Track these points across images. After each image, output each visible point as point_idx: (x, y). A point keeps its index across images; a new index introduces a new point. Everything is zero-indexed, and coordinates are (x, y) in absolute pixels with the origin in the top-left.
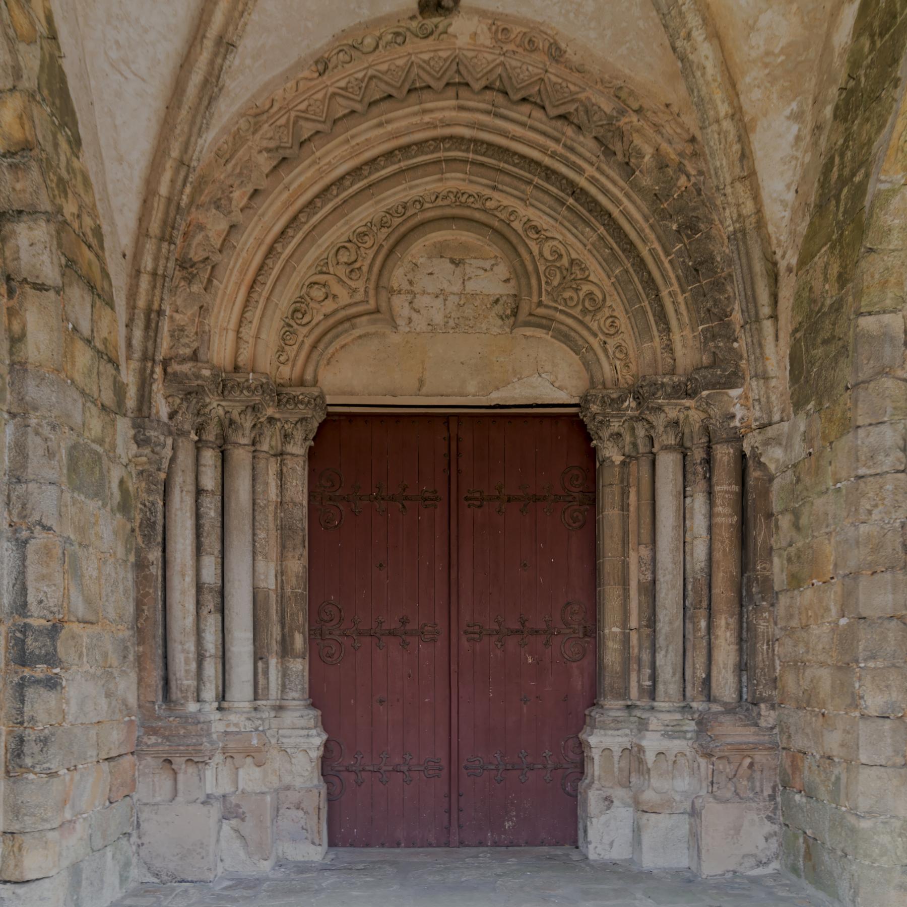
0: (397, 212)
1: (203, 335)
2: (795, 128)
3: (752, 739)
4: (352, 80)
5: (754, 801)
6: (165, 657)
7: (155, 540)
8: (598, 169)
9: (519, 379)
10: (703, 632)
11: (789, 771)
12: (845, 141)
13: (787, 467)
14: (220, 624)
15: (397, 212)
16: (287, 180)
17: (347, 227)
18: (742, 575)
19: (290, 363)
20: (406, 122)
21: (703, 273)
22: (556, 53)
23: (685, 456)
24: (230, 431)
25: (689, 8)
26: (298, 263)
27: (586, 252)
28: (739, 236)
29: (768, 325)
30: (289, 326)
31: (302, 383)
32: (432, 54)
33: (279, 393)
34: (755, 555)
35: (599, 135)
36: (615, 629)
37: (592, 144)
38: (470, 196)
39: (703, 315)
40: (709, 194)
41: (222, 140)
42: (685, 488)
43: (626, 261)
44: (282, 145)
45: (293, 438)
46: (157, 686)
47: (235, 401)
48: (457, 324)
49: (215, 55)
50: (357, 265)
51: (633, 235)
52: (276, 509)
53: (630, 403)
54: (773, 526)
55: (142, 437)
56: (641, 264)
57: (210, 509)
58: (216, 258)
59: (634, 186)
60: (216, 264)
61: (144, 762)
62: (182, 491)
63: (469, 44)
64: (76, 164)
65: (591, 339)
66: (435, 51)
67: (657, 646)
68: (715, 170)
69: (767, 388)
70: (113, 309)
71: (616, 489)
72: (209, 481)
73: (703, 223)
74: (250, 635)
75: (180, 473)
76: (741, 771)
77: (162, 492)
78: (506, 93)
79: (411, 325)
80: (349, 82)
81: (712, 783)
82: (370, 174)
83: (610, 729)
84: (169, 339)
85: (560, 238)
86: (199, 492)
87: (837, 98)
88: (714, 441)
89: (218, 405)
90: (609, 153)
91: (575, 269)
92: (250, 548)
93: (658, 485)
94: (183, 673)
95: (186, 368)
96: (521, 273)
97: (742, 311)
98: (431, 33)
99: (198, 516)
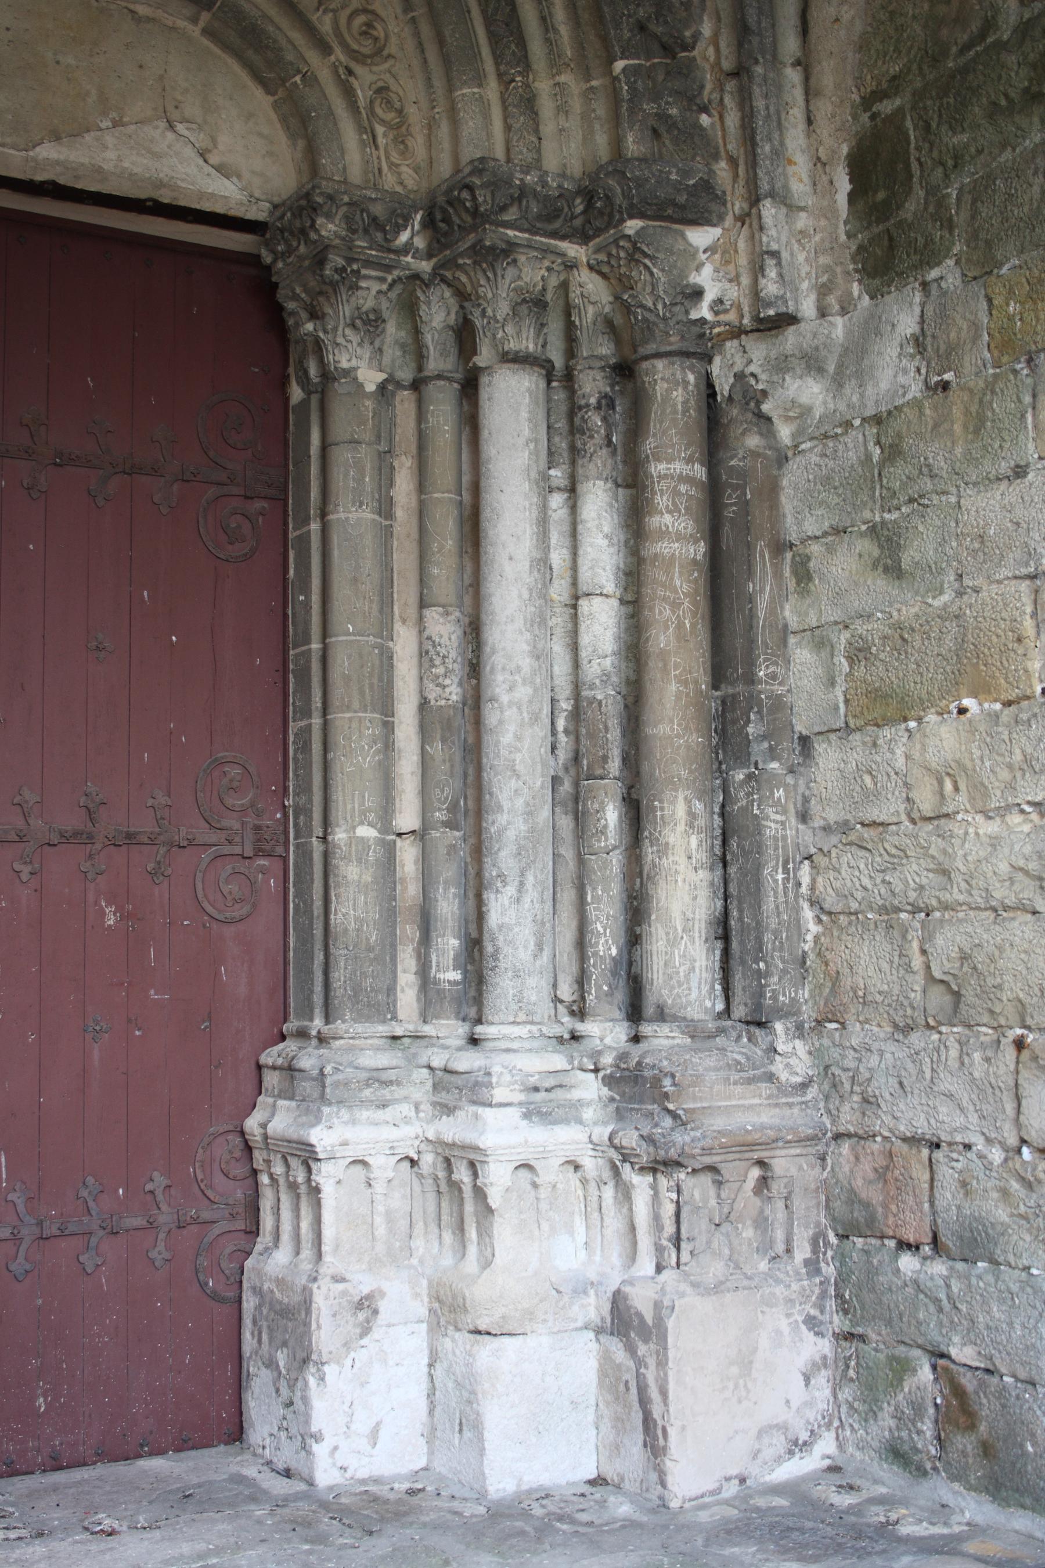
5: (778, 1281)
9: (116, 124)
13: (848, 424)
34: (751, 642)
39: (627, 34)
65: (313, 57)
71: (366, 454)
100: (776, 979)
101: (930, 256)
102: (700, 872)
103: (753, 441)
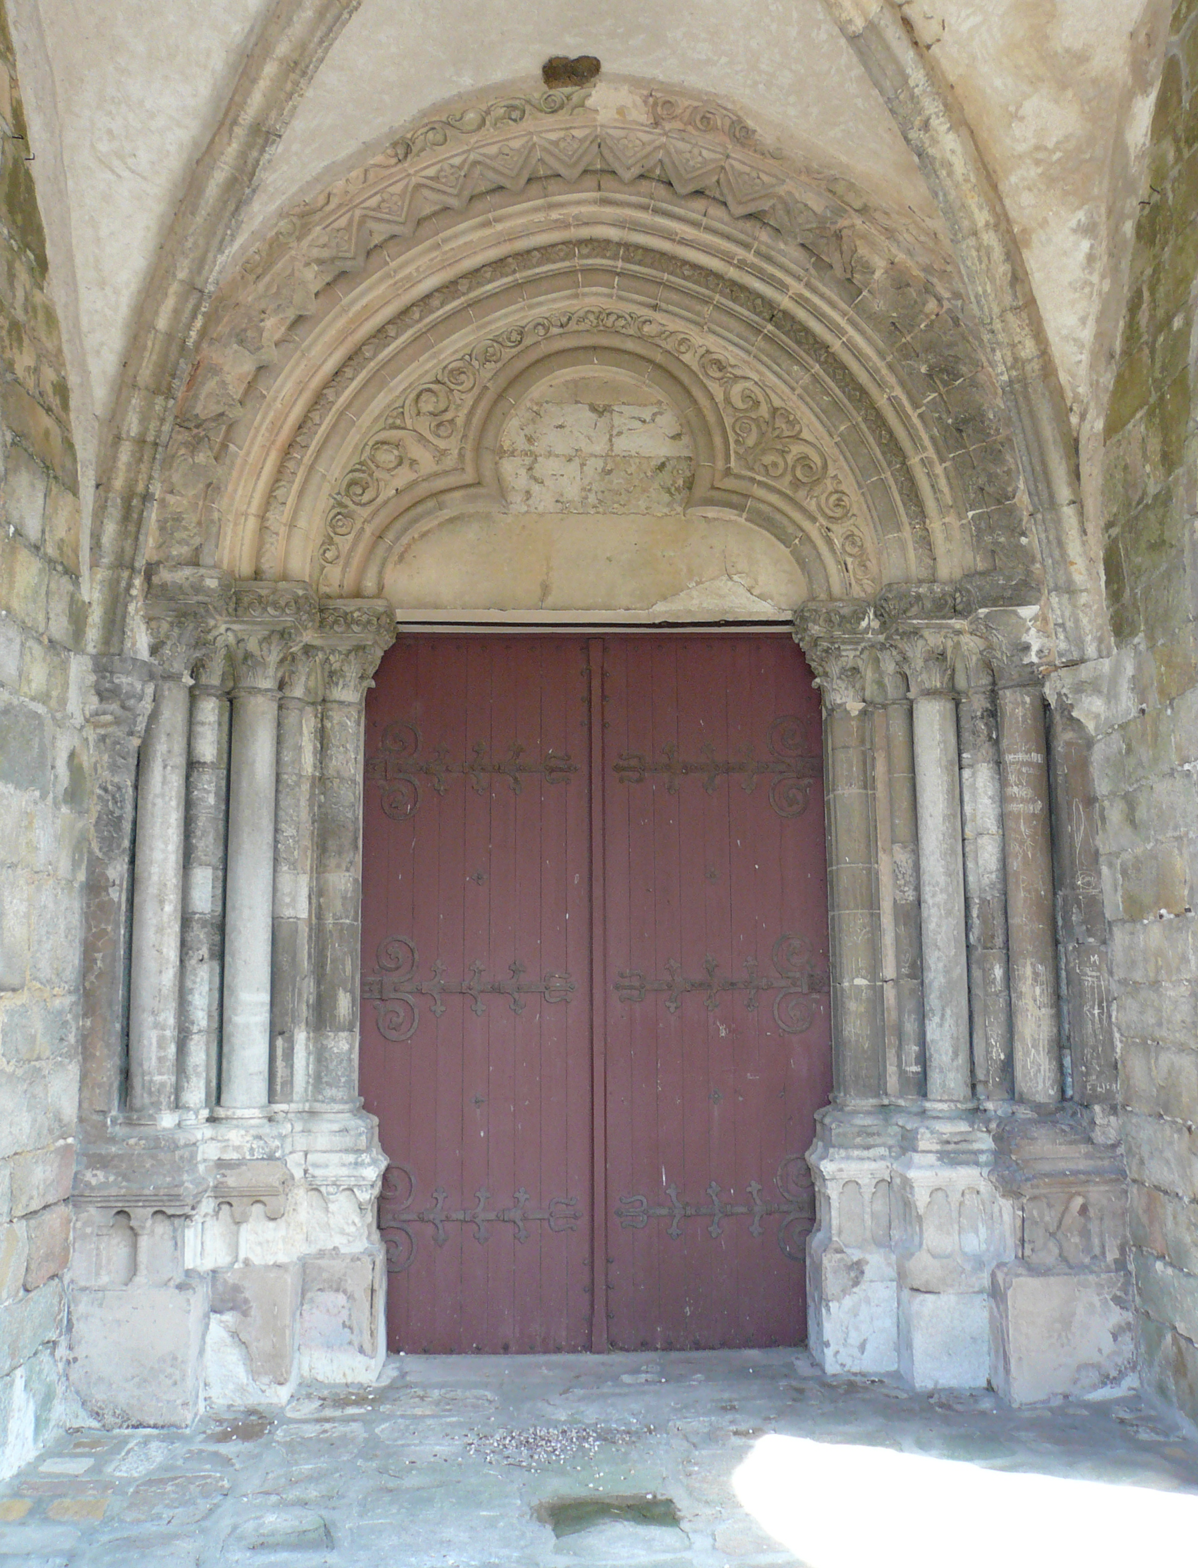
0: (509, 339)
1: (210, 527)
2: (1085, 245)
3: (1083, 1165)
4: (446, 167)
5: (1092, 1272)
6: (126, 1033)
7: (119, 846)
8: (808, 285)
9: (697, 584)
10: (999, 985)
11: (1145, 1219)
12: (1154, 271)
13: (1112, 727)
14: (217, 980)
15: (509, 339)
16: (346, 300)
17: (435, 361)
18: (1055, 894)
19: (341, 561)
20: (526, 222)
21: (968, 433)
22: (741, 133)
23: (957, 704)
24: (245, 668)
25: (924, 91)
26: (358, 415)
27: (795, 398)
28: (1018, 389)
29: (1068, 512)
30: (341, 504)
31: (358, 594)
32: (562, 134)
33: (322, 610)
34: (1073, 863)
35: (806, 242)
36: (859, 981)
37: (797, 253)
38: (619, 317)
39: (973, 496)
40: (971, 325)
41: (254, 249)
42: (959, 755)
43: (854, 413)
44: (340, 254)
45: (344, 677)
46: (111, 1085)
47: (255, 623)
48: (600, 501)
49: (249, 146)
50: (448, 416)
51: (863, 377)
52: (313, 786)
53: (869, 621)
54: (1097, 817)
55: (107, 685)
56: (878, 421)
57: (208, 792)
58: (236, 413)
59: (861, 310)
60: (236, 422)
61: (84, 1215)
62: (165, 767)
63: (615, 120)
64: (38, 297)
65: (807, 525)
66: (567, 129)
67: (927, 1008)
68: (976, 298)
69: (1075, 606)
70: (75, 494)
71: (854, 755)
72: (208, 748)
73: (965, 364)
74: (266, 997)
75: (163, 738)
76: (1068, 1220)
77: (133, 768)
78: (670, 184)
79: (530, 502)
80: (441, 170)
81: (1023, 1241)
82: (470, 289)
83: (857, 1147)
84: (157, 533)
85: (756, 378)
86: (192, 765)
87: (1138, 214)
88: (1001, 683)
89: (227, 630)
90: (823, 266)
91: (780, 423)
92: (270, 855)
93: (919, 750)
94: (154, 1061)
95: (183, 575)
96: (697, 425)
97: (1030, 494)
98: (562, 107)
99: (189, 805)
100: (1094, 1077)
101: (1133, 634)
102: (1043, 1010)
103: (1069, 735)
